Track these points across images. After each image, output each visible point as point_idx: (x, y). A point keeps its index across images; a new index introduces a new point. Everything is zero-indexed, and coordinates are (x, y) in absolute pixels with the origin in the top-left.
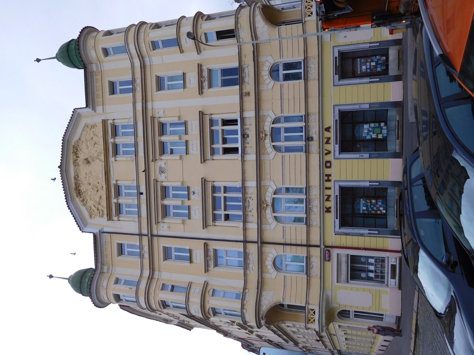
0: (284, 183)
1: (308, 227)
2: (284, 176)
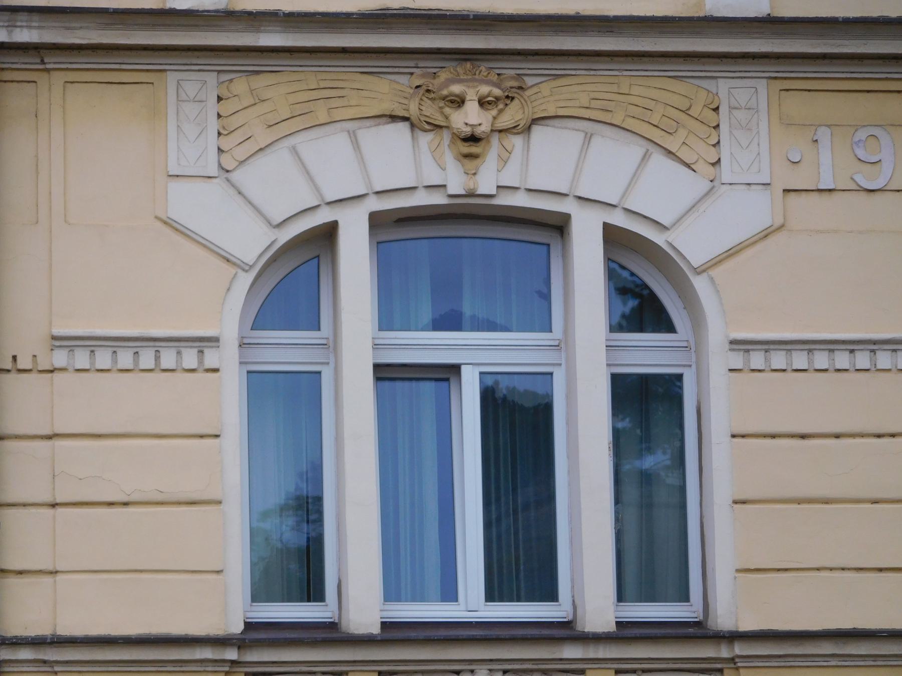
0: (757, 359)
1: (232, 654)
2: (842, 360)
